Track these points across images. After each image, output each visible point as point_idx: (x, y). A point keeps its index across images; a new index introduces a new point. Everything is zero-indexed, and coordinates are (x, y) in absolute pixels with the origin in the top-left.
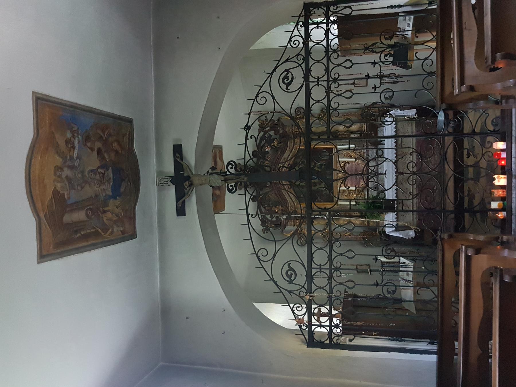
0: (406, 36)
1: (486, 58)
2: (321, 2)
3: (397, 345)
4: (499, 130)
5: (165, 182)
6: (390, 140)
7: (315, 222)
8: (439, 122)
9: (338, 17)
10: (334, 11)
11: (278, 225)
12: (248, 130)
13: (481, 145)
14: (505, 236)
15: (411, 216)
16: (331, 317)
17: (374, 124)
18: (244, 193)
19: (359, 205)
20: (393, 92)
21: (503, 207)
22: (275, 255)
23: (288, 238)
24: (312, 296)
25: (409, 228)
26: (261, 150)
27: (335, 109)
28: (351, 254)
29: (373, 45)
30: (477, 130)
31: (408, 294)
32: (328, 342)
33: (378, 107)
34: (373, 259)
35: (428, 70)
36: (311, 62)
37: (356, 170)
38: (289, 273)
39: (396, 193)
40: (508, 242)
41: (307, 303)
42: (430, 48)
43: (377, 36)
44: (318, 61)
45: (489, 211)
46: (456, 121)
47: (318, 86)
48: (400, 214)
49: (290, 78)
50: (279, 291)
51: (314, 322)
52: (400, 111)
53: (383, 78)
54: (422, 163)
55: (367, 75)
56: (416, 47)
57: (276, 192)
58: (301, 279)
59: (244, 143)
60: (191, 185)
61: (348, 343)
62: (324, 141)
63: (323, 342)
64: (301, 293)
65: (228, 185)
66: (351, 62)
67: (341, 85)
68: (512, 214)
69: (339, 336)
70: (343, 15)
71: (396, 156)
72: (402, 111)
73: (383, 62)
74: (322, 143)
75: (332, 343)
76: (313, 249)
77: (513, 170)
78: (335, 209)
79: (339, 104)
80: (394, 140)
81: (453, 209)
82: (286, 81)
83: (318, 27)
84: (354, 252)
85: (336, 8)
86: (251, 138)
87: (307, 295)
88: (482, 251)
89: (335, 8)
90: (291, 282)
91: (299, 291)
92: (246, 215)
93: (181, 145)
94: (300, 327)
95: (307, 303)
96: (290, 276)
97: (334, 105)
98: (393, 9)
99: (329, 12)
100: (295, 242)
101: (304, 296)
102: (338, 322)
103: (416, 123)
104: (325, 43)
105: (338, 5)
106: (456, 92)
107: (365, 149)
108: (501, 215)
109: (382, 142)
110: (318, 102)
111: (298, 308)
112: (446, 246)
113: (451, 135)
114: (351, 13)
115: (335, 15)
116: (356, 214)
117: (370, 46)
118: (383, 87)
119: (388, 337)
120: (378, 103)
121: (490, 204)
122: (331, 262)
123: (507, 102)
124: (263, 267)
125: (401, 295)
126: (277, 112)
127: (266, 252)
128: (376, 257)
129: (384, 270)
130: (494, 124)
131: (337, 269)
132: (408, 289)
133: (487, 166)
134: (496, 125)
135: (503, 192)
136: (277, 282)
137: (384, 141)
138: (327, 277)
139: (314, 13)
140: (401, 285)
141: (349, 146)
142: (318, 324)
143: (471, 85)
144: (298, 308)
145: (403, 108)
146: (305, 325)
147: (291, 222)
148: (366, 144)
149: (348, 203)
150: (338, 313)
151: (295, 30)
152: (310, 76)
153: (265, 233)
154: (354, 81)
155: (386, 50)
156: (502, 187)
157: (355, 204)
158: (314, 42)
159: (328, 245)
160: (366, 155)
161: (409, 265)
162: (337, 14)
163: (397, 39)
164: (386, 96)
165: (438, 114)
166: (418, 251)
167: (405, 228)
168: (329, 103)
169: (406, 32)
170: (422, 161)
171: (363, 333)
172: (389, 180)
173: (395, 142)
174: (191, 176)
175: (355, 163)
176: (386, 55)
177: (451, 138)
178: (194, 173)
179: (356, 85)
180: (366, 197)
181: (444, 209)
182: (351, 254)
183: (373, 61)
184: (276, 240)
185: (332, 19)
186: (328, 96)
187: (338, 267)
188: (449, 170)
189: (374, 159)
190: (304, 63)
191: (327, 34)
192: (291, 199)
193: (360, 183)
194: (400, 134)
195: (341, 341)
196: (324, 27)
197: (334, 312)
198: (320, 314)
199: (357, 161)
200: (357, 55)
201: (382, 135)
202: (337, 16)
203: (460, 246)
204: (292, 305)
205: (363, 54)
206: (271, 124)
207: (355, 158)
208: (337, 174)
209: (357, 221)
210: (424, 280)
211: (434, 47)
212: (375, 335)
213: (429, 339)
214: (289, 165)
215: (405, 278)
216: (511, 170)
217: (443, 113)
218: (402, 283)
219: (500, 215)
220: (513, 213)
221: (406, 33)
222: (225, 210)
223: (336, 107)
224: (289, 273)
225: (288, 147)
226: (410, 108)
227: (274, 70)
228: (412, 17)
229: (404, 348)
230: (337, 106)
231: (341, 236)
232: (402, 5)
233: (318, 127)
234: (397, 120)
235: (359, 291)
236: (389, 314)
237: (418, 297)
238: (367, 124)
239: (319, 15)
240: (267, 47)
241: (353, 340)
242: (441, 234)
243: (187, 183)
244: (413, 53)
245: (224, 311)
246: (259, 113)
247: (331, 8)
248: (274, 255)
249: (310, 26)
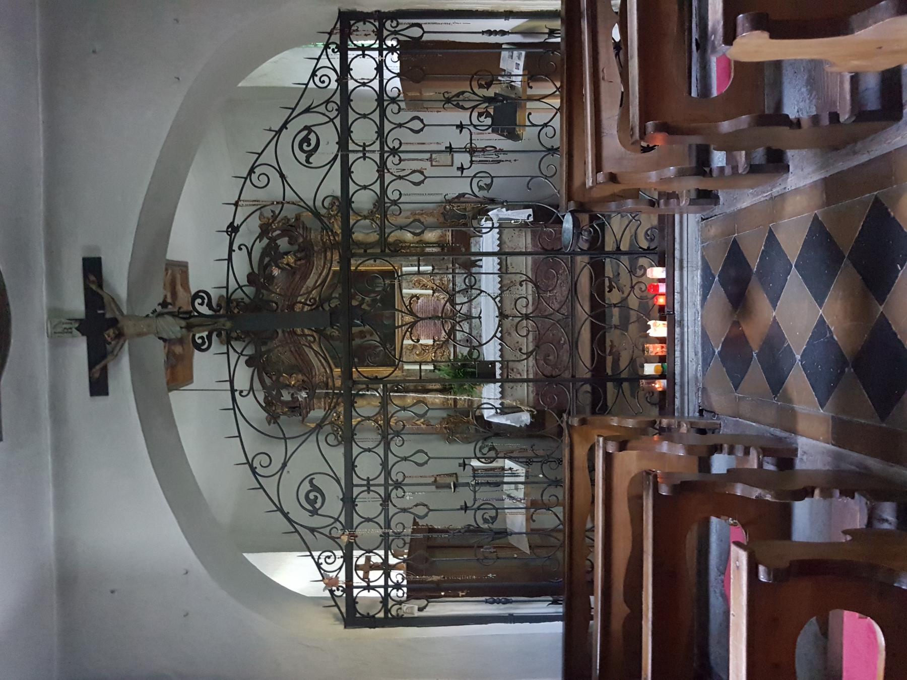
0: (513, 83)
1: (632, 129)
2: (369, 11)
3: (500, 609)
4: (656, 248)
5: (66, 331)
6: (490, 258)
7: (360, 403)
8: (565, 232)
9: (399, 41)
10: (393, 29)
11: (295, 408)
12: (233, 234)
13: (629, 272)
14: (665, 418)
16: (386, 569)
17: (463, 231)
18: (226, 351)
19: (439, 370)
20: (492, 177)
21: (663, 372)
22: (284, 465)
23: (311, 432)
24: (353, 535)
25: (516, 410)
26: (265, 272)
27: (395, 202)
28: (420, 458)
29: (458, 95)
30: (624, 247)
31: (517, 521)
32: (381, 615)
33: (468, 202)
34: (460, 465)
35: (548, 143)
36: (352, 116)
37: (435, 309)
38: (311, 496)
39: (500, 350)
40: (669, 428)
41: (344, 548)
42: (551, 107)
43: (465, 80)
44: (365, 116)
45: (642, 379)
46: (590, 231)
47: (365, 159)
48: (507, 385)
49: (313, 142)
50: (294, 530)
51: (357, 581)
52: (507, 210)
53: (474, 153)
54: (539, 298)
55: (449, 145)
56: (529, 105)
57: (292, 349)
58: (333, 506)
59: (227, 258)
60: (120, 335)
61: (417, 614)
62: (375, 257)
63: (373, 616)
64: (334, 531)
65: (194, 336)
66: (422, 121)
67: (404, 160)
68: (675, 384)
69: (400, 603)
70: (409, 39)
71: (501, 287)
72: (509, 211)
73: (475, 126)
74: (372, 262)
75: (390, 616)
76: (356, 450)
77: (675, 312)
78: (398, 379)
79: (400, 194)
80: (496, 260)
81: (589, 375)
82: (305, 147)
83: (364, 55)
84: (426, 454)
85: (395, 25)
86: (240, 249)
87: (344, 533)
88: (629, 445)
89: (394, 24)
90: (314, 512)
91: (329, 528)
92: (230, 392)
93: (99, 259)
94: (332, 592)
95: (344, 548)
96: (312, 502)
97: (392, 195)
98: (492, 36)
99: (384, 30)
100: (321, 438)
101: (339, 536)
102: (400, 578)
103: (532, 231)
104: (375, 84)
105: (400, 21)
106: (589, 183)
107: (450, 273)
108: (660, 385)
109: (478, 263)
110: (365, 187)
111: (327, 560)
112: (576, 438)
113: (584, 254)
114: (422, 36)
115: (393, 36)
116: (435, 387)
117: (453, 97)
118: (476, 168)
119: (483, 598)
120: (467, 196)
121: (643, 367)
122: (388, 474)
123: (667, 204)
124: (262, 487)
125: (505, 521)
126: (288, 203)
127: (268, 458)
128: (464, 461)
129: (478, 483)
130: (648, 238)
131: (398, 485)
132: (517, 514)
133: (639, 306)
134: (652, 240)
135: (662, 347)
136: (288, 513)
137: (481, 260)
138: (380, 499)
139: (357, 30)
140: (505, 507)
141: (419, 269)
142: (365, 584)
143: (611, 173)
144: (327, 560)
145: (511, 206)
146: (341, 589)
147: (320, 403)
148: (451, 265)
149: (417, 367)
150: (401, 563)
151: (322, 57)
152: (350, 141)
153: (272, 425)
154: (431, 155)
155: (480, 106)
156: (661, 340)
157: (433, 368)
158: (356, 81)
159: (382, 443)
160: (451, 284)
161: (518, 472)
162: (397, 36)
163: (500, 89)
164: (481, 184)
165: (564, 218)
166: (533, 447)
167: (515, 410)
168: (384, 190)
169: (514, 77)
170: (538, 296)
171: (443, 594)
172: (489, 325)
173: (498, 264)
174: (119, 318)
175: (433, 298)
176: (480, 115)
177: (586, 259)
178: (125, 312)
179: (434, 163)
180: (452, 357)
181: (573, 376)
182: (420, 458)
183: (459, 123)
184: (286, 436)
185: (389, 43)
186: (381, 177)
187: (400, 480)
188: (583, 309)
189: (464, 291)
190: (339, 117)
191: (380, 68)
194: (507, 251)
195: (404, 612)
196: (374, 57)
197: (392, 561)
198: (369, 567)
199: (437, 294)
200: (431, 110)
201: (478, 250)
202: (396, 38)
203: (596, 437)
204: (316, 554)
205: (443, 109)
206: (284, 224)
208: (402, 317)
209: (436, 398)
210: (542, 497)
211: (557, 107)
212: (463, 596)
213: (551, 595)
214: (312, 301)
215: (512, 495)
216: (674, 313)
217: (571, 217)
218: (508, 502)
219: (657, 386)
220: (676, 381)
221: (514, 79)
222: (192, 382)
223: (396, 199)
224: (311, 496)
226: (522, 207)
227: (284, 126)
228: (523, 53)
229: (511, 615)
230: (398, 196)
231: (404, 426)
232: (507, 30)
233: (364, 233)
234: (503, 226)
235: (436, 521)
236: (486, 558)
237: (534, 526)
238: (452, 231)
239: (366, 35)
240: (274, 84)
241: (425, 607)
242: (568, 418)
243: (111, 332)
244: (526, 112)
245: (187, 573)
246: (257, 203)
247: (388, 24)
248: (283, 464)
249: (349, 52)
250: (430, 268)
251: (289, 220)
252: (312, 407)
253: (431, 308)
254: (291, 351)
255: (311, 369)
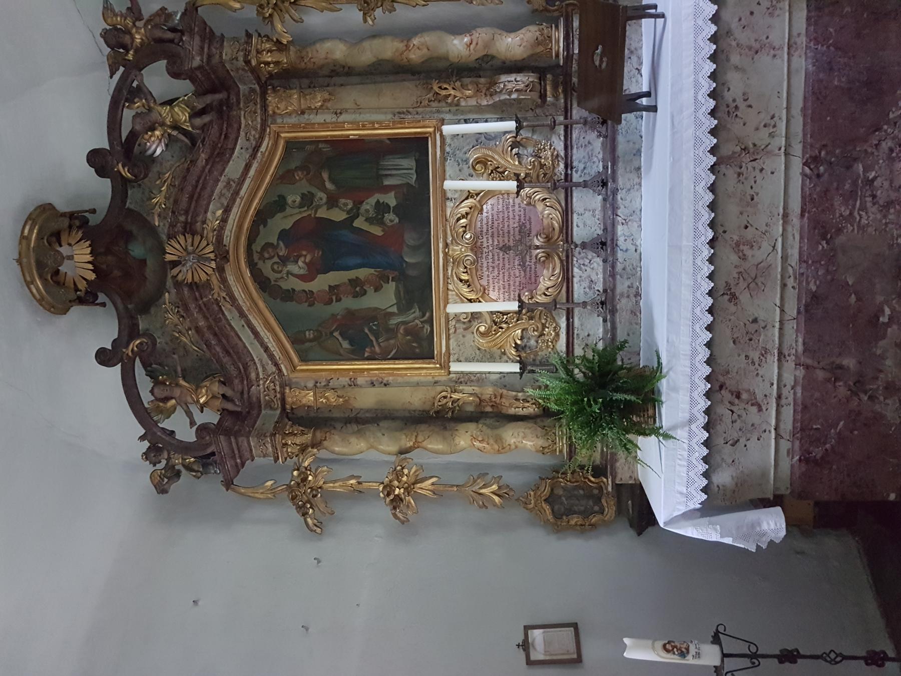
15: (769, 445)
37: (522, 226)
160: (562, 166)
175: (518, 201)
192: (266, 349)
193: (536, 283)
207: (517, 177)
225: (242, 134)
250: (511, 125)
251: (169, 16)
252: (247, 454)
253: (514, 224)
254: (198, 330)
255: (246, 367)
